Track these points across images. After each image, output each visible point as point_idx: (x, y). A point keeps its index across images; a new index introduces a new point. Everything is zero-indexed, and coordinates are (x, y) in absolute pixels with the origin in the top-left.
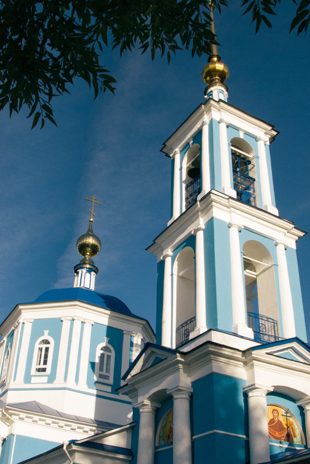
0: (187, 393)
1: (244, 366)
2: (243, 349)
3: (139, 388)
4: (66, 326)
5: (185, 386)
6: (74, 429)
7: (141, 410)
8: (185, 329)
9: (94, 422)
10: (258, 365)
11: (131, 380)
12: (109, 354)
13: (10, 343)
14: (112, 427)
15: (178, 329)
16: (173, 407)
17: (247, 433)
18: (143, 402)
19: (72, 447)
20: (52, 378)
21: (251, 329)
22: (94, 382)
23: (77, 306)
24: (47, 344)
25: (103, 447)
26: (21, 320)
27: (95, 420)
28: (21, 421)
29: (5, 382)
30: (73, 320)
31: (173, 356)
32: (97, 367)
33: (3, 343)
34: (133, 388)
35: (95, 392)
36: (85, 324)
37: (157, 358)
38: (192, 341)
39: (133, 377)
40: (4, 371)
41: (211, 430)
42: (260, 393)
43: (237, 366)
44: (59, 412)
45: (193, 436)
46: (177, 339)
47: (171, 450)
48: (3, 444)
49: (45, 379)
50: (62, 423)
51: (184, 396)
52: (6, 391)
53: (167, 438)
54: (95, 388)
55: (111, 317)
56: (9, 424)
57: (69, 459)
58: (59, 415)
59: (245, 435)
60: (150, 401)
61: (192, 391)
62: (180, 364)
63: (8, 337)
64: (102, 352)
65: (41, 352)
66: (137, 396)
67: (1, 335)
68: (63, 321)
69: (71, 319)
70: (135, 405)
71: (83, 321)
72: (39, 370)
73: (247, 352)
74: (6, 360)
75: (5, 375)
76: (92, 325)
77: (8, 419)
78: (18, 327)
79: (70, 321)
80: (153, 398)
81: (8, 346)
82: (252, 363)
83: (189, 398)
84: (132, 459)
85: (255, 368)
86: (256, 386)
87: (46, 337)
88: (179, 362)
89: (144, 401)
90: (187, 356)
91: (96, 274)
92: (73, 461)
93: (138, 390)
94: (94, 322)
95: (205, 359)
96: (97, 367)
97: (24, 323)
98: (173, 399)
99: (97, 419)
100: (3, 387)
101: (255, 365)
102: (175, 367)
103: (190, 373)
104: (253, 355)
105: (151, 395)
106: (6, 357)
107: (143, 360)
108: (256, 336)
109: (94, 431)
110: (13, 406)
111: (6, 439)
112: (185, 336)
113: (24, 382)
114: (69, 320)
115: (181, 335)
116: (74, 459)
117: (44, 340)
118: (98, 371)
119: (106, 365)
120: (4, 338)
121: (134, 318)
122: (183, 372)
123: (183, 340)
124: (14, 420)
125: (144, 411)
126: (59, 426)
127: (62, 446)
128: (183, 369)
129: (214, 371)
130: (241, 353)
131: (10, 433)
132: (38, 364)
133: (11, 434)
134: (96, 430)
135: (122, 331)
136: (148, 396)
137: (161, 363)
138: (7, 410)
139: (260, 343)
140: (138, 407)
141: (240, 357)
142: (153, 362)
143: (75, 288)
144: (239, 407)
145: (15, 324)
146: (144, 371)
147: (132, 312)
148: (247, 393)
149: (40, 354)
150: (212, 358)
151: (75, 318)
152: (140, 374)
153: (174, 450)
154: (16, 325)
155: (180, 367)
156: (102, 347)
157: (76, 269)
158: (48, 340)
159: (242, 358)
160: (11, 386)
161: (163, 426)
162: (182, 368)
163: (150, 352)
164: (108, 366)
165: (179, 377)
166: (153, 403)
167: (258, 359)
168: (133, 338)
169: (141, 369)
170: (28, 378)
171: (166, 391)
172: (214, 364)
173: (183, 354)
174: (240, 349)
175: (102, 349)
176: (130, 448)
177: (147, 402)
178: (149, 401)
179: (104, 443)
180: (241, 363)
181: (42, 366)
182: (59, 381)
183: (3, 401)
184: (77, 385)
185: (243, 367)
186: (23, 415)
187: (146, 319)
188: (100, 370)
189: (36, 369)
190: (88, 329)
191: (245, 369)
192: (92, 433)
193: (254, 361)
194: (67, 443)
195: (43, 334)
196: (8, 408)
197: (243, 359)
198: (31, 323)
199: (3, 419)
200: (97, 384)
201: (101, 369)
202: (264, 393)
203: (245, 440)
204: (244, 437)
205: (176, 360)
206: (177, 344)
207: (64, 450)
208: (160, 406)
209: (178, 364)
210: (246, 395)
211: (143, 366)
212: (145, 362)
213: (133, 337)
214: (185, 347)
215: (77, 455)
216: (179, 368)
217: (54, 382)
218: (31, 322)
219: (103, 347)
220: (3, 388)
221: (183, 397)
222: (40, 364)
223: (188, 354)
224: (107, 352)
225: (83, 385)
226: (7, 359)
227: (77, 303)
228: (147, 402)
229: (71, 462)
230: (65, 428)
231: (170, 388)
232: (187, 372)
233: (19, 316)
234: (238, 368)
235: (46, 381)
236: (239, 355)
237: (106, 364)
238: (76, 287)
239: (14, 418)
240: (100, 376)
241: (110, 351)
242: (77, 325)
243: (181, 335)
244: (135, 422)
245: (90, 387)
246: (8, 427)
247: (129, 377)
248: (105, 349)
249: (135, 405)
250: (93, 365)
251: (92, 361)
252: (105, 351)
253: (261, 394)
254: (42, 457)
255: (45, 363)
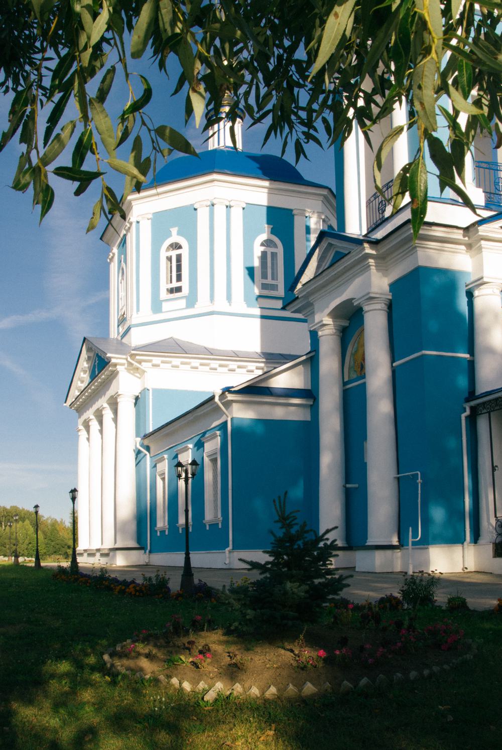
0: (381, 302)
1: (468, 251)
2: (465, 226)
3: (315, 301)
4: (203, 216)
5: (379, 291)
6: (233, 370)
7: (320, 333)
8: (380, 200)
9: (260, 356)
10: (488, 247)
11: (302, 291)
12: (274, 250)
13: (123, 256)
14: (287, 359)
15: (369, 203)
16: (363, 323)
17: (471, 350)
18: (322, 321)
19: (227, 397)
20: (192, 301)
21: (481, 190)
22: (255, 298)
23: (216, 182)
24: (178, 249)
25: (270, 391)
26: (133, 217)
27: (262, 353)
28: (156, 369)
29: (125, 316)
30: (213, 205)
31: (361, 248)
32: (258, 274)
33: (113, 257)
34: (306, 302)
35: (257, 311)
36: (232, 208)
37: (337, 253)
38: (381, 226)
39: (306, 286)
40: (121, 299)
41: (417, 352)
42: (492, 289)
43: (456, 252)
44: (210, 349)
45: (394, 362)
46: (369, 219)
47: (364, 385)
48: (135, 404)
49: (183, 303)
50: (215, 364)
51: (378, 306)
52: (129, 329)
53: (360, 369)
54: (258, 306)
55: (271, 191)
56: (140, 374)
57: (225, 413)
58: (209, 353)
59: (468, 353)
60: (332, 318)
61: (390, 297)
62: (370, 259)
63: (119, 247)
64: (263, 249)
65: (171, 263)
66: (313, 313)
67: (108, 244)
68: (198, 209)
69: (209, 203)
70: (312, 327)
71: (228, 204)
72: (171, 291)
73: (471, 229)
74: (121, 283)
75: (124, 305)
76: (244, 209)
77: (138, 369)
78: (131, 230)
79: (208, 208)
80: (335, 314)
81: (121, 261)
82: (479, 245)
83: (386, 308)
84: (314, 402)
85: (483, 253)
86: (485, 280)
87: (175, 238)
88: (368, 256)
89: (324, 319)
90: (379, 246)
91: (242, 120)
92: (230, 415)
93: (314, 304)
94: (246, 203)
95: (407, 247)
96: (258, 274)
97: (138, 222)
98: (363, 312)
99: (263, 352)
100: (122, 323)
101: (484, 248)
102: (409, 246)
103: (387, 270)
104: (480, 233)
105: (333, 309)
106: (120, 278)
107: (317, 259)
108: (489, 200)
109: (262, 369)
110: (143, 349)
111: (138, 396)
112: (380, 211)
113: (151, 311)
114: (207, 206)
115: (374, 210)
116: (231, 413)
117: (173, 243)
118: (259, 280)
119: (270, 270)
120: (113, 249)
121: (310, 188)
122: (375, 271)
123: (378, 219)
124: (145, 369)
125: (324, 334)
126: (211, 369)
127: (212, 398)
128: (375, 266)
129: (420, 265)
130: (461, 232)
131: (143, 388)
132: (169, 282)
133: (145, 389)
134: (265, 366)
135: (292, 210)
136: (329, 312)
137: (343, 260)
138: (133, 356)
139: (495, 211)
140: (315, 329)
141: (461, 237)
142: (330, 263)
143: (211, 151)
144: (460, 316)
145: (126, 226)
146: (319, 275)
147: (306, 178)
148: (472, 291)
149: (169, 267)
150: (416, 245)
151: (215, 202)
152: (315, 280)
153: (367, 385)
154: (127, 228)
155: (370, 264)
156: (262, 241)
157: (208, 117)
158: (178, 244)
159: (463, 238)
160: (134, 321)
161: (353, 351)
162: (374, 264)
163: (326, 245)
164: (275, 269)
165: (369, 278)
166: (334, 320)
167: (488, 238)
168: (309, 220)
169: (316, 272)
170: (157, 306)
171: (353, 301)
172: (420, 253)
173: (375, 243)
174: (459, 226)
175: (262, 245)
176: (309, 388)
177: (328, 320)
178: (330, 318)
179: (270, 386)
180: (463, 247)
181: (175, 284)
182: (202, 304)
183: (126, 344)
184: (230, 305)
185: (467, 252)
186: (156, 360)
187: (327, 185)
188: (262, 278)
189: (167, 289)
190: (237, 215)
191: (468, 256)
192: (260, 372)
193: (483, 242)
194: (218, 392)
195: (170, 235)
196: (134, 354)
197: (465, 240)
198: (150, 220)
199: (130, 369)
200: (262, 300)
201: (264, 276)
202: (497, 289)
203: (468, 361)
204: (467, 356)
205: (363, 253)
206: (369, 226)
207: (216, 403)
208: (347, 324)
209: (368, 259)
210: (470, 295)
211: (318, 267)
212: (321, 260)
213: (310, 218)
214: (378, 232)
215: (235, 406)
216: (370, 266)
217: (196, 306)
218: (148, 219)
219: (264, 241)
220: (124, 325)
221: (377, 308)
222: (171, 282)
223: (381, 242)
224: (271, 247)
225: (239, 304)
226: (122, 281)
227: (215, 176)
228: (327, 320)
229: (228, 417)
230: (220, 369)
231: (357, 297)
232: (381, 270)
233: (130, 211)
234: (458, 254)
235: (184, 306)
236: (458, 235)
237: (270, 267)
238: (212, 149)
239: (144, 366)
240: (264, 286)
241: (276, 246)
242: (220, 211)
243: (374, 210)
244: (315, 351)
245: (249, 305)
246: (138, 379)
247: (299, 286)
248: (267, 243)
249: (312, 327)
250: (251, 271)
251: (250, 265)
252: (268, 246)
253: (493, 291)
254: (190, 414)
255: (179, 278)
